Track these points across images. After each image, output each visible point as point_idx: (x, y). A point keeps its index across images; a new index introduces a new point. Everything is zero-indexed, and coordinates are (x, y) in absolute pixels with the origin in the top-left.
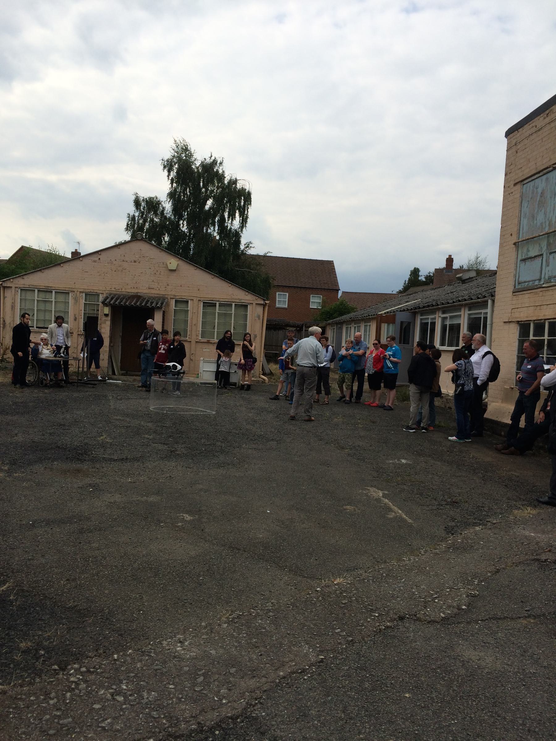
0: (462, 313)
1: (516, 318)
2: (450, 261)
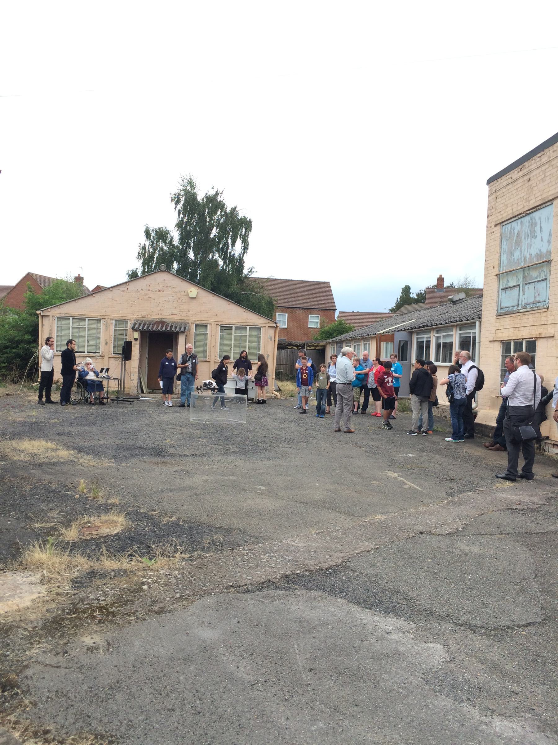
0: (454, 333)
1: (500, 337)
2: (441, 280)
